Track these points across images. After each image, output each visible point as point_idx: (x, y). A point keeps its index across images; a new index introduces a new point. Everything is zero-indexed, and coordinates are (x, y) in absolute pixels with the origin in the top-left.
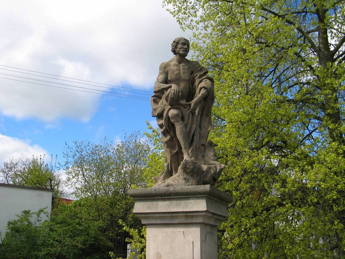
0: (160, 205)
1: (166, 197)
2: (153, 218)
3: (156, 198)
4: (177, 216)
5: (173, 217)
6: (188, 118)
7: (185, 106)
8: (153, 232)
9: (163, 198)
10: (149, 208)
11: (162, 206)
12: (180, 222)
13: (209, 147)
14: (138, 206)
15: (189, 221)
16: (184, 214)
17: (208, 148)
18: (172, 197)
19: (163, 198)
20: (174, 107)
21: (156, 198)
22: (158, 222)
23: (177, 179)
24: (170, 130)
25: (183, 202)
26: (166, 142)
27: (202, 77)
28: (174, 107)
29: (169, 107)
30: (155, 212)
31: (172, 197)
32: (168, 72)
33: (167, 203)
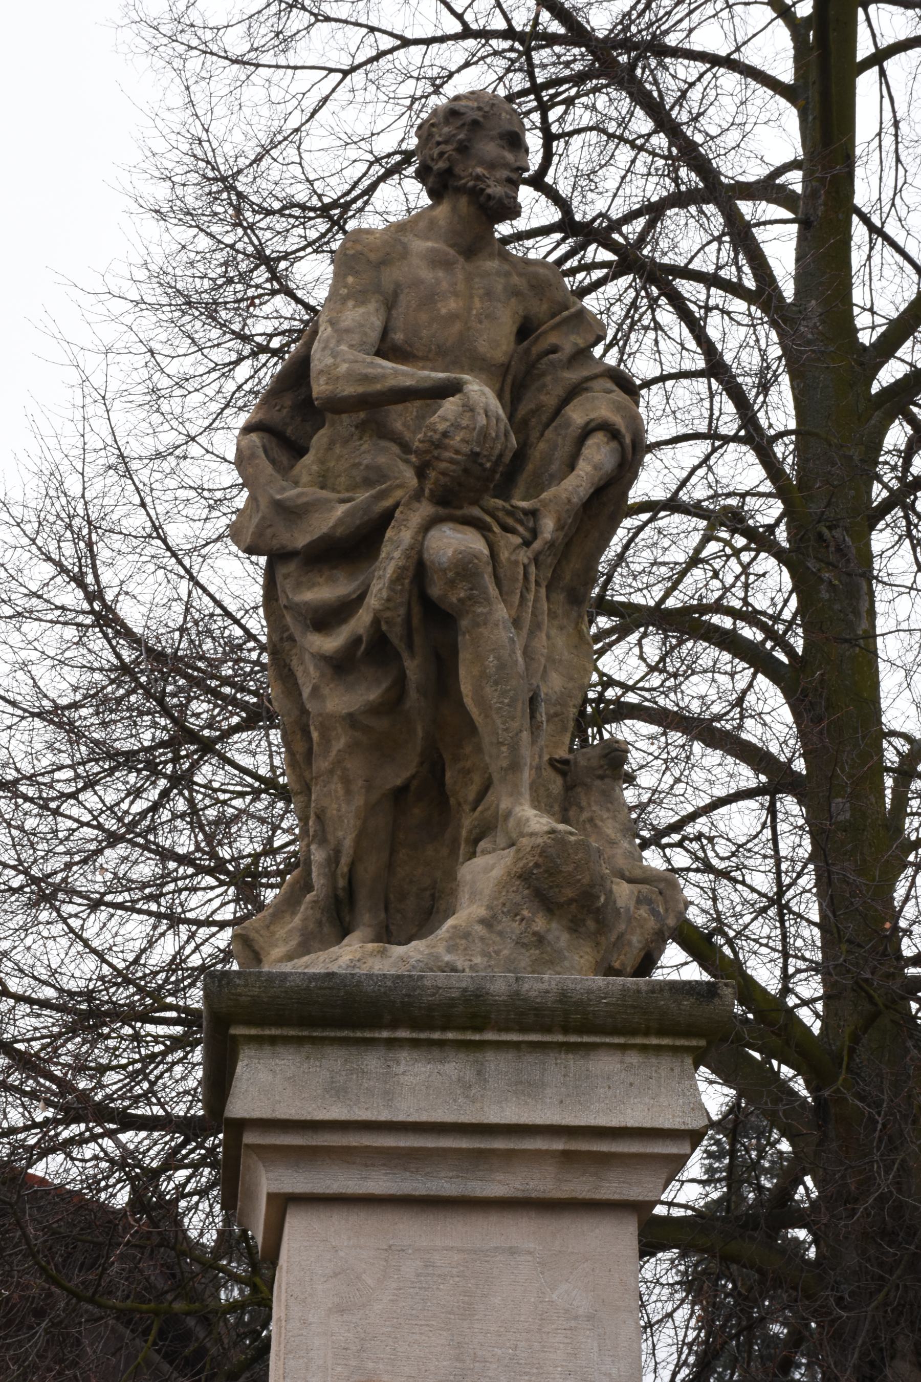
0: (408, 1079)
1: (450, 1035)
2: (345, 1155)
3: (385, 1034)
4: (509, 1155)
5: (479, 1159)
6: (522, 596)
7: (510, 521)
8: (335, 1249)
9: (436, 1035)
10: (337, 1092)
11: (419, 1087)
12: (519, 1194)
13: (601, 778)
14: (264, 1076)
15: (580, 1186)
16: (559, 1145)
17: (598, 783)
18: (490, 1036)
19: (436, 1035)
20: (459, 513)
21: (385, 1034)
22: (379, 1183)
23: (482, 939)
24: (410, 646)
25: (557, 1071)
26: (351, 715)
27: (448, 379)
28: (459, 513)
29: (425, 510)
30: (382, 1118)
31: (490, 1036)
32: (396, 295)
33: (453, 1068)
